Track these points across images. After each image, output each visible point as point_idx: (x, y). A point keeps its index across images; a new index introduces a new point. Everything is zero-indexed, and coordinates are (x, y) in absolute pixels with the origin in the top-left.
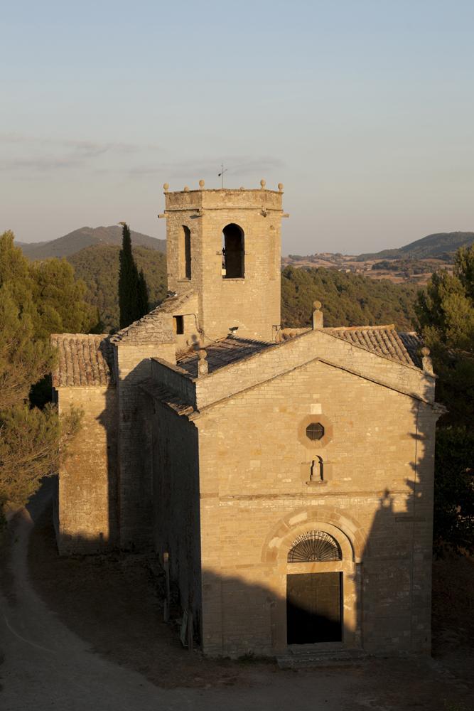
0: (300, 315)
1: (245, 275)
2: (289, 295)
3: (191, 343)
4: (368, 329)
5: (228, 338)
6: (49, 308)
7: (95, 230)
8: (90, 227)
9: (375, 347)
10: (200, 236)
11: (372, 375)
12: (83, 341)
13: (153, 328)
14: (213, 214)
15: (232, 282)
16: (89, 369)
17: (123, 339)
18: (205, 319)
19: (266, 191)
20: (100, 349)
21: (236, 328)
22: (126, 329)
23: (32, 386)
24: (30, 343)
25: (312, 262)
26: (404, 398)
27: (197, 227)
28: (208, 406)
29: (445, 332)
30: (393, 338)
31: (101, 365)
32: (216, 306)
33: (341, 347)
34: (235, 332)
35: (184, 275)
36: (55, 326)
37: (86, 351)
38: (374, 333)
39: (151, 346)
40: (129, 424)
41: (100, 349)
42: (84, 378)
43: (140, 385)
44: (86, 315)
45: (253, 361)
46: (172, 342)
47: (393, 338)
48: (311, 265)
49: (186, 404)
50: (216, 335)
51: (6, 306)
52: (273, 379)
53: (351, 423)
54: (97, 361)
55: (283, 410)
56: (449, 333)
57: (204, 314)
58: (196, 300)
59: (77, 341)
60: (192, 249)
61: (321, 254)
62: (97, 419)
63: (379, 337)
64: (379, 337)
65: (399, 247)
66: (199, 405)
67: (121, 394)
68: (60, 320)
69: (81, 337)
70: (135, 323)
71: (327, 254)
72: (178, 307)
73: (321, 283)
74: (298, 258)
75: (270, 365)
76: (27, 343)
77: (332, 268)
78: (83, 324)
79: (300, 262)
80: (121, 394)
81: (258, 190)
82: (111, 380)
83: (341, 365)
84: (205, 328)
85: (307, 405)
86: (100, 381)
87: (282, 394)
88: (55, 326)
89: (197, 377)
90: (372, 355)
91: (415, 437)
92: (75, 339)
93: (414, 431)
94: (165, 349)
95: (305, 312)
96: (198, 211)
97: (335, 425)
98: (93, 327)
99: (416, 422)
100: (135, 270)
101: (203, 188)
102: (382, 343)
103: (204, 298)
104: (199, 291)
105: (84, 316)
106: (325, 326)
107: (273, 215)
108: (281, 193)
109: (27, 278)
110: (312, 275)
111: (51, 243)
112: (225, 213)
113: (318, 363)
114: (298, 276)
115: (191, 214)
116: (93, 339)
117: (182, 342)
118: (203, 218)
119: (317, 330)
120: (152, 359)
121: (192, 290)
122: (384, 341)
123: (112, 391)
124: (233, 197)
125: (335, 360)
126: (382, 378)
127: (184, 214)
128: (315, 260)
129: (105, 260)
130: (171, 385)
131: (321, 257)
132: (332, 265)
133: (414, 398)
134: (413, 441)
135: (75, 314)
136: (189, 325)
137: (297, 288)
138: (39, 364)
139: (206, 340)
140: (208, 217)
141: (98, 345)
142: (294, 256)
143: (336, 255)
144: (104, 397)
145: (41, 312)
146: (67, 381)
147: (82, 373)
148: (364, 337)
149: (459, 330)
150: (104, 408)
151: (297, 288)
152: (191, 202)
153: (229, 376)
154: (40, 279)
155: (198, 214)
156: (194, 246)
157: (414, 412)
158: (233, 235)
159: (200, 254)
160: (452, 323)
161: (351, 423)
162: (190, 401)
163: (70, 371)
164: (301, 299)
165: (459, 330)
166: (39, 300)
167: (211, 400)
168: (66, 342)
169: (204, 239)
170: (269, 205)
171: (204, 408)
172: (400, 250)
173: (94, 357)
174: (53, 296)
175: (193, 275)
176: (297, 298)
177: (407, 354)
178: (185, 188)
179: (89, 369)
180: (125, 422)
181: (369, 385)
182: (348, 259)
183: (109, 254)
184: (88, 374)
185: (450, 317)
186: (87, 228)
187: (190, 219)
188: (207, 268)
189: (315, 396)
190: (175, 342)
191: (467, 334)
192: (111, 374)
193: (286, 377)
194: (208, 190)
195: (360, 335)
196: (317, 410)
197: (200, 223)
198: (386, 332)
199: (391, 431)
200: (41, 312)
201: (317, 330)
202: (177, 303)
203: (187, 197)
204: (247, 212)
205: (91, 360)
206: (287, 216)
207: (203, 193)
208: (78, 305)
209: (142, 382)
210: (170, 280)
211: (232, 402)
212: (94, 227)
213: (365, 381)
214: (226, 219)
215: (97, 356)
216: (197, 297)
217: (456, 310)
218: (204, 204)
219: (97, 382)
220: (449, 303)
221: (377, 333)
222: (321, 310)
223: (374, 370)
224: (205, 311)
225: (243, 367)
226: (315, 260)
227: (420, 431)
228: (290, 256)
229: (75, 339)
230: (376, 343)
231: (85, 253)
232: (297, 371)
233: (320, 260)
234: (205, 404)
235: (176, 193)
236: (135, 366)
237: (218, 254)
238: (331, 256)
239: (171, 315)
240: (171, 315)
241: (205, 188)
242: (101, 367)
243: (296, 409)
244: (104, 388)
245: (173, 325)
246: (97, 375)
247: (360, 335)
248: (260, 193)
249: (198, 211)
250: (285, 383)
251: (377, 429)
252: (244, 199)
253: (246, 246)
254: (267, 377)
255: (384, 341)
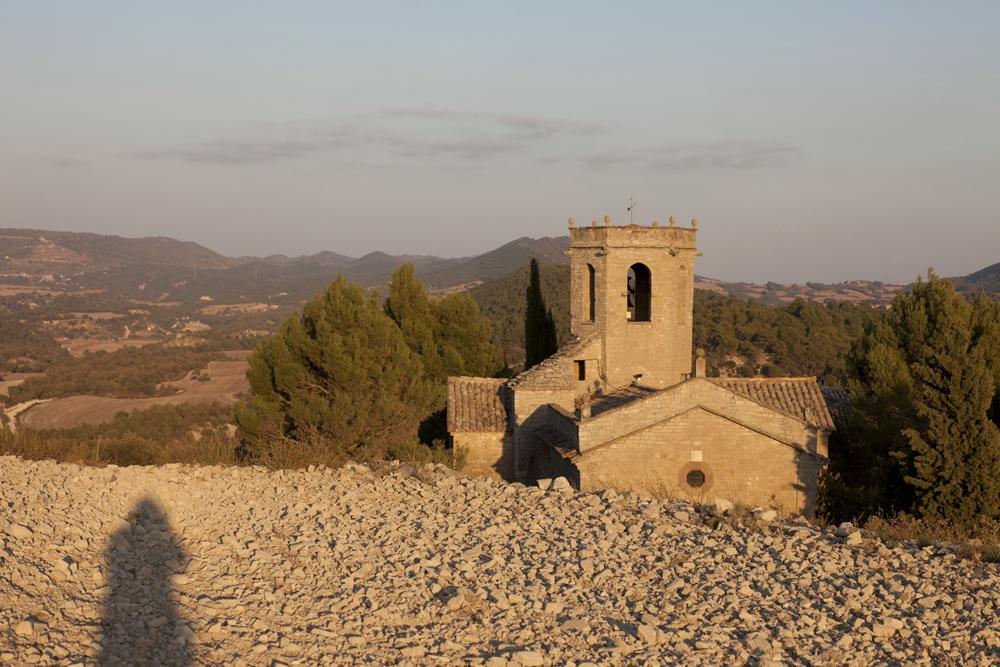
0: (809, 368)
1: (651, 318)
2: (795, 340)
3: (593, 389)
4: (787, 381)
5: (631, 386)
6: (450, 349)
7: (537, 241)
8: (531, 237)
9: (792, 400)
10: (604, 275)
11: (754, 423)
12: (482, 385)
13: (552, 373)
14: (619, 252)
15: (638, 325)
16: (486, 415)
17: (521, 383)
18: (608, 364)
19: (675, 228)
20: (498, 394)
21: (640, 376)
22: (526, 373)
23: (422, 423)
24: (420, 382)
25: (840, 292)
26: (786, 448)
27: (602, 267)
28: (590, 450)
29: (869, 385)
30: (813, 392)
31: (498, 411)
32: (611, 347)
33: (723, 395)
34: (639, 379)
35: (588, 318)
36: (456, 369)
37: (484, 395)
38: (793, 385)
39: (549, 392)
40: (525, 472)
41: (498, 394)
42: (480, 423)
43: (740, 525)
44: (491, 357)
45: (636, 406)
46: (570, 388)
47: (813, 392)
48: (839, 298)
49: (572, 448)
50: (619, 383)
51: (398, 346)
52: (654, 425)
53: (732, 472)
54: (495, 406)
55: (664, 456)
56: (875, 387)
57: (608, 360)
58: (599, 345)
59: (475, 384)
60: (596, 290)
61: (852, 282)
62: (494, 466)
63: (798, 390)
64: (798, 390)
65: (965, 273)
66: (582, 447)
67: (517, 441)
68: (462, 362)
69: (479, 380)
70: (534, 367)
71: (861, 282)
72: (579, 351)
73: (842, 325)
74: (819, 287)
75: (652, 411)
76: (417, 382)
77: (862, 303)
78: (487, 367)
79: (822, 293)
80: (517, 441)
81: (667, 228)
82: (508, 426)
83: (723, 413)
84: (608, 374)
85: (688, 452)
86: (497, 428)
87: (664, 440)
88: (456, 369)
89: (580, 421)
90: (754, 404)
91: (797, 487)
92: (472, 382)
93: (796, 481)
94: (564, 395)
95: (817, 364)
96: (602, 248)
97: (715, 472)
98: (498, 371)
99: (798, 473)
100: (542, 309)
101: (607, 225)
102: (800, 396)
103: (607, 343)
104: (603, 336)
105: (488, 359)
106: (707, 376)
107: (682, 254)
108: (694, 230)
109: (427, 315)
110: (833, 312)
111: (477, 258)
112: (631, 252)
113: (700, 410)
114: (811, 313)
115: (595, 251)
116: (492, 383)
117: (583, 388)
118: (608, 257)
119: (699, 378)
120: (549, 406)
121: (595, 333)
122: (803, 394)
123: (509, 439)
124: (640, 234)
125: (716, 408)
126: (764, 427)
127: (589, 252)
128: (845, 290)
129: (548, 284)
130: (562, 430)
131: (853, 286)
132: (866, 298)
133: (797, 449)
134: (794, 492)
135: (479, 356)
136: (592, 372)
137: (808, 330)
138: (428, 403)
139: (608, 387)
140: (613, 254)
141: (497, 389)
142: (815, 284)
143: (875, 284)
144: (501, 444)
145: (441, 353)
146: (462, 426)
147: (479, 418)
148: (781, 389)
149: (885, 385)
150: (500, 456)
151: (808, 330)
152: (596, 240)
153: (610, 420)
154: (442, 316)
155: (602, 252)
156: (598, 286)
157: (796, 462)
158: (641, 274)
159: (604, 295)
160: (876, 376)
161: (732, 472)
162: (574, 444)
163: (467, 416)
164: (812, 345)
165: (885, 385)
166: (440, 341)
167: (593, 444)
168: (463, 386)
169: (608, 280)
170: (679, 243)
171: (586, 451)
172: (967, 279)
173: (491, 401)
174: (455, 336)
175: (596, 318)
176: (806, 344)
177: (826, 409)
178: (594, 223)
179: (486, 415)
180: (521, 470)
181: (750, 434)
182: (891, 289)
183: (555, 277)
184: (485, 420)
185: (875, 370)
186: (527, 239)
187: (595, 258)
188: (611, 310)
189: (697, 443)
190: (575, 388)
191: (892, 388)
192: (508, 419)
193: (668, 424)
194: (614, 227)
195: (777, 387)
196: (698, 457)
197: (604, 262)
198: (806, 384)
199: (771, 481)
200: (441, 353)
201: (699, 378)
202: (579, 346)
203: (592, 233)
204: (655, 251)
205: (488, 405)
206: (701, 255)
207: (608, 230)
208: (482, 346)
209: (538, 430)
210: (573, 322)
211: (614, 446)
212: (537, 237)
213: (747, 430)
214: (634, 257)
215: (495, 401)
216: (600, 341)
217: (882, 362)
218: (609, 242)
219: (493, 428)
220: (876, 354)
221: (797, 385)
222: (704, 357)
223: (757, 420)
224: (608, 356)
225: (626, 412)
226: (845, 290)
227: (802, 481)
228: (808, 284)
229: (472, 382)
230: (794, 396)
231: (523, 274)
232: (678, 417)
233: (851, 291)
234: (587, 448)
235: (581, 229)
236: (532, 412)
237: (623, 295)
238: (866, 285)
239: (571, 360)
240: (571, 360)
241: (610, 224)
242: (498, 413)
243: (677, 455)
244: (501, 435)
245: (574, 370)
246: (493, 421)
247: (777, 387)
248: (669, 231)
249: (602, 248)
250: (666, 429)
251: (757, 478)
252: (652, 236)
253: (653, 287)
254: (648, 422)
255: (803, 394)
